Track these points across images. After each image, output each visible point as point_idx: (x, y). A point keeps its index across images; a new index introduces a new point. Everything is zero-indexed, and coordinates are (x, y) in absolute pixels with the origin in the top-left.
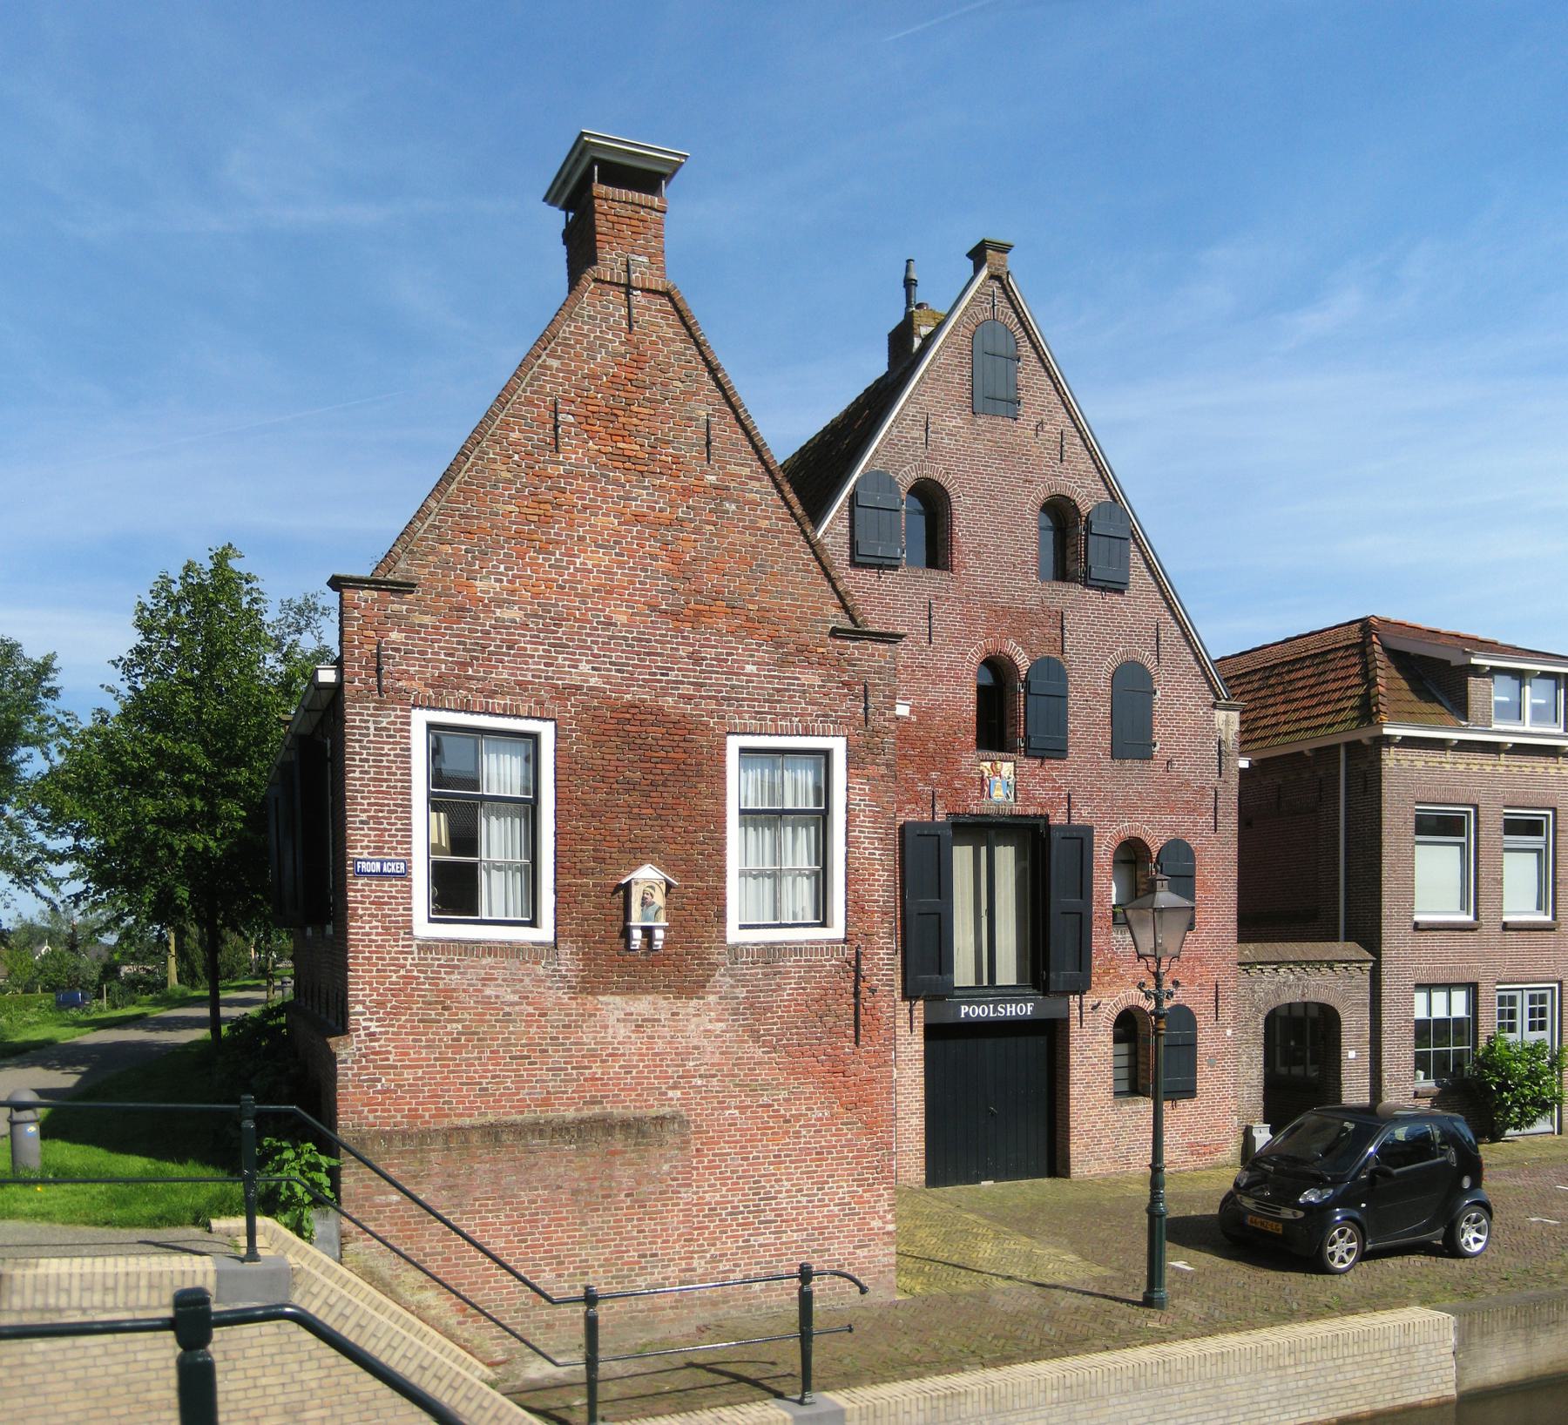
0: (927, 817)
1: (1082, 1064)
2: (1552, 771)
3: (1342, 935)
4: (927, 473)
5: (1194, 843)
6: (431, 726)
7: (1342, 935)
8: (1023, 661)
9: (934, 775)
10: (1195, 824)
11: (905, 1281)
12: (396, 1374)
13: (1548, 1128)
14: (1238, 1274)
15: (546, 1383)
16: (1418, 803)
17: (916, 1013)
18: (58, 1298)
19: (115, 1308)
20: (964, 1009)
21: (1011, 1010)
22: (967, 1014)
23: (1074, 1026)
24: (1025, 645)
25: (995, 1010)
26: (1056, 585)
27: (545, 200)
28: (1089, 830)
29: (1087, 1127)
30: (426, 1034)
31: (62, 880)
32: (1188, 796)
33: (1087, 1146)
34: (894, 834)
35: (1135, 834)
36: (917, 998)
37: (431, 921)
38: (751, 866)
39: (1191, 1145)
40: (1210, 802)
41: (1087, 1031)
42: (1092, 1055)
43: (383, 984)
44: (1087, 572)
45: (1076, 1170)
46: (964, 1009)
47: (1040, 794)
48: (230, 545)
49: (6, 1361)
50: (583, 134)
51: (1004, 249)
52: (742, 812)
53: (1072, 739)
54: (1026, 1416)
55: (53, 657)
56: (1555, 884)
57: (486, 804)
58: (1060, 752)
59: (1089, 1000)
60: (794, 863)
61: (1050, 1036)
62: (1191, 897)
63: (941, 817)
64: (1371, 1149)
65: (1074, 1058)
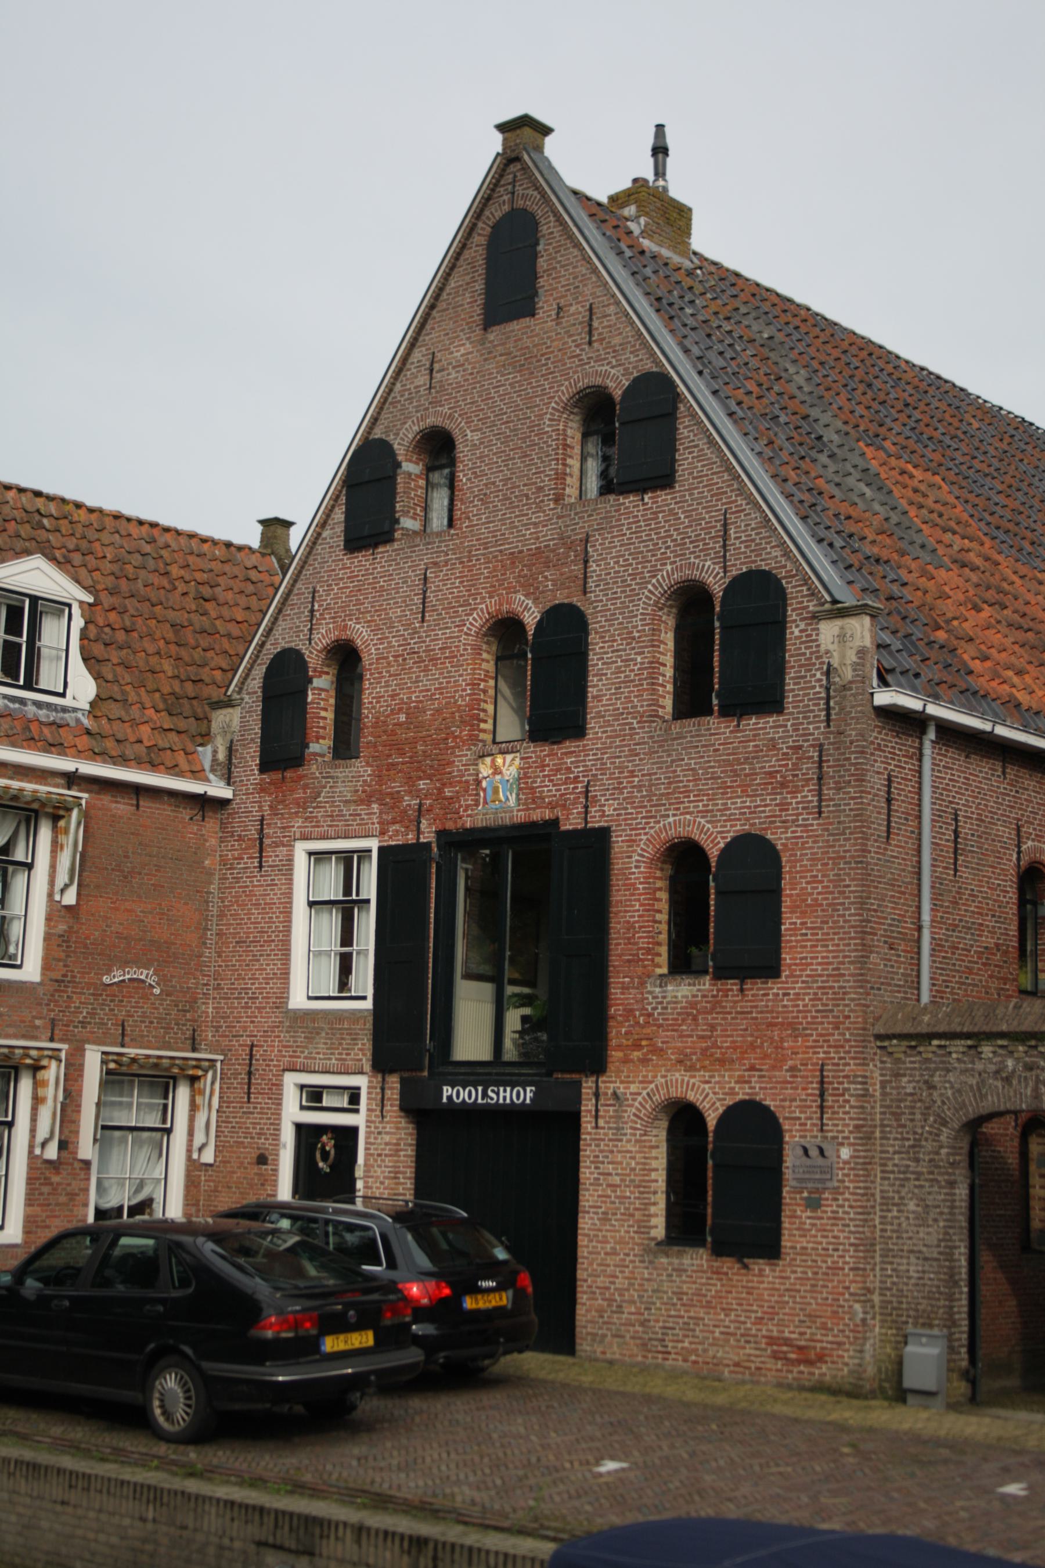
0: (411, 838)
1: (596, 1183)
4: (430, 421)
5: (778, 838)
8: (531, 618)
9: (422, 784)
10: (784, 806)
12: (505, 828)
13: (471, 1042)
17: (388, 1093)
18: (484, 731)
19: (655, 664)
20: (447, 1091)
21: (505, 1096)
22: (450, 1098)
23: (587, 1123)
24: (534, 594)
25: (485, 1095)
28: (603, 835)
29: (601, 1281)
30: (822, 928)
32: (772, 763)
33: (601, 1312)
34: (947, 1147)
35: (683, 832)
36: (392, 1071)
37: (302, 1108)
39: (771, 1341)
40: (809, 769)
41: (606, 1131)
42: (622, 1171)
43: (827, 922)
44: (106, 1104)
45: (584, 1346)
46: (447, 1091)
47: (549, 790)
50: (69, 606)
52: (311, 904)
53: (594, 708)
56: (139, 790)
58: (771, 969)
59: (609, 1084)
60: (358, 894)
61: (553, 1135)
63: (428, 836)
65: (587, 1173)
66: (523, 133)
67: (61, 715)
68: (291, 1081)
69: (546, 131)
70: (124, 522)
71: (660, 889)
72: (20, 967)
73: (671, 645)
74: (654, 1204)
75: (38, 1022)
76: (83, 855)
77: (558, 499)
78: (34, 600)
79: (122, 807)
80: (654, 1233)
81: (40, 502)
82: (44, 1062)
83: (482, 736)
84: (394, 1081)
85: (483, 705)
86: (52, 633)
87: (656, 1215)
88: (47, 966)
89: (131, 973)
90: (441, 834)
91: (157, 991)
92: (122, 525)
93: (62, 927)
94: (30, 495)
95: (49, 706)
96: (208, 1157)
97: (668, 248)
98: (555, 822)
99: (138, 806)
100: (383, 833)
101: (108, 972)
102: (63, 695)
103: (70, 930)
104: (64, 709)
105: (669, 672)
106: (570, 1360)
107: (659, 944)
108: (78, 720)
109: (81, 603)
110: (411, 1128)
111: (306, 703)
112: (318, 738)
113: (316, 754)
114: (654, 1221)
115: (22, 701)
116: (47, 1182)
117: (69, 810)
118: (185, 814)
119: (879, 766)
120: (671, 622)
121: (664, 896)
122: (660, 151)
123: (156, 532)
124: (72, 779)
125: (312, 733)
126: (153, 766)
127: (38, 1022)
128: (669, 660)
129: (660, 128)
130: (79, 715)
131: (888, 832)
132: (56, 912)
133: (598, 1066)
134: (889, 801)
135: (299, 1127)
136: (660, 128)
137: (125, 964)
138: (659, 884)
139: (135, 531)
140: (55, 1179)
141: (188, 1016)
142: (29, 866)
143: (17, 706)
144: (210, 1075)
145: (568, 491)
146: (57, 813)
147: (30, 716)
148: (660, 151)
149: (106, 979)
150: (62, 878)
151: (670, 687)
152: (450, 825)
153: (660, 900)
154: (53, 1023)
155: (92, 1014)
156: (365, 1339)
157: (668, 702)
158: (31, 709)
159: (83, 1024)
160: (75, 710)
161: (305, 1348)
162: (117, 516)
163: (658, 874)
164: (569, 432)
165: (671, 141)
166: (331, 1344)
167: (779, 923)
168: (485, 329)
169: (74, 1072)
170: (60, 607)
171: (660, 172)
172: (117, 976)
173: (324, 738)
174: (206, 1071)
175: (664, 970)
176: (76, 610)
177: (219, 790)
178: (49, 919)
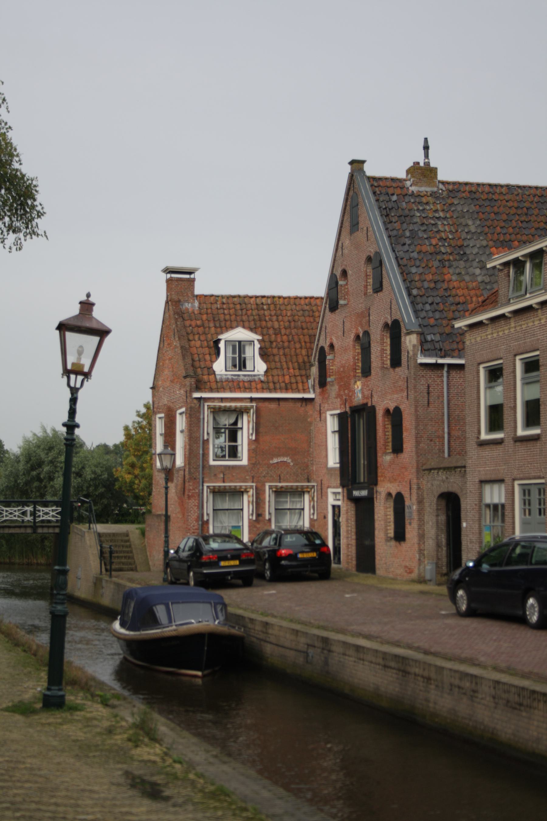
2: (478, 339)
3: (207, 636)
6: (269, 486)
7: (207, 636)
11: (120, 766)
14: (383, 265)
15: (531, 438)
16: (461, 367)
18: (358, 373)
20: (274, 592)
26: (466, 369)
27: (168, 271)
31: (419, 311)
38: (463, 469)
48: (37, 178)
49: (543, 219)
50: (253, 341)
51: (23, 709)
54: (42, 773)
55: (197, 270)
57: (334, 272)
62: (52, 613)
63: (348, 409)
64: (206, 648)
66: (357, 165)
67: (253, 378)
68: (330, 491)
69: (363, 162)
70: (298, 300)
71: (388, 424)
72: (241, 460)
73: (389, 343)
74: (389, 526)
75: (247, 477)
76: (256, 423)
77: (365, 294)
78: (240, 342)
79: (273, 406)
80: (389, 535)
81: (264, 300)
82: (248, 490)
83: (357, 375)
84: (345, 489)
85: (357, 364)
86: (249, 352)
87: (390, 530)
88: (249, 459)
89: (285, 459)
90: (350, 407)
91: (292, 464)
92: (297, 301)
93: (253, 447)
94: (260, 298)
95: (249, 375)
96: (315, 517)
97: (426, 186)
98: (367, 404)
99: (279, 405)
100: (340, 408)
101: (272, 459)
102: (254, 371)
103: (257, 447)
104: (255, 375)
105: (388, 352)
106: (374, 576)
107: (388, 442)
108: (259, 379)
109: (258, 340)
110: (353, 505)
111: (326, 365)
112: (330, 376)
113: (329, 382)
114: (389, 531)
115: (239, 375)
116: (255, 527)
117: (250, 410)
118: (299, 404)
119: (423, 382)
120: (388, 335)
121: (390, 426)
122: (426, 148)
123: (312, 300)
124: (252, 400)
125: (328, 374)
126: (286, 389)
127: (247, 477)
128: (388, 348)
129: (426, 140)
130: (261, 377)
131: (428, 403)
132: (250, 442)
133: (376, 484)
134: (428, 393)
135: (334, 507)
136: (426, 140)
137: (278, 456)
138: (387, 423)
139: (302, 302)
140: (258, 526)
141: (305, 471)
142: (242, 428)
143: (236, 377)
144: (313, 490)
145: (368, 291)
146: (247, 410)
147: (241, 380)
148: (426, 148)
149: (271, 462)
150: (251, 431)
151: (389, 357)
152: (351, 405)
153: (388, 428)
154: (253, 477)
155: (268, 473)
156: (237, 562)
157: (389, 362)
158: (242, 377)
159: (264, 477)
160: (259, 375)
161: (215, 564)
162: (296, 298)
163: (386, 419)
164: (368, 270)
165: (430, 144)
166: (222, 563)
167: (402, 435)
168: (351, 235)
169: (259, 493)
170: (251, 342)
171: (427, 156)
172: (275, 461)
173: (333, 376)
174: (311, 489)
175: (391, 451)
176: (256, 343)
177: (311, 395)
178: (249, 444)
